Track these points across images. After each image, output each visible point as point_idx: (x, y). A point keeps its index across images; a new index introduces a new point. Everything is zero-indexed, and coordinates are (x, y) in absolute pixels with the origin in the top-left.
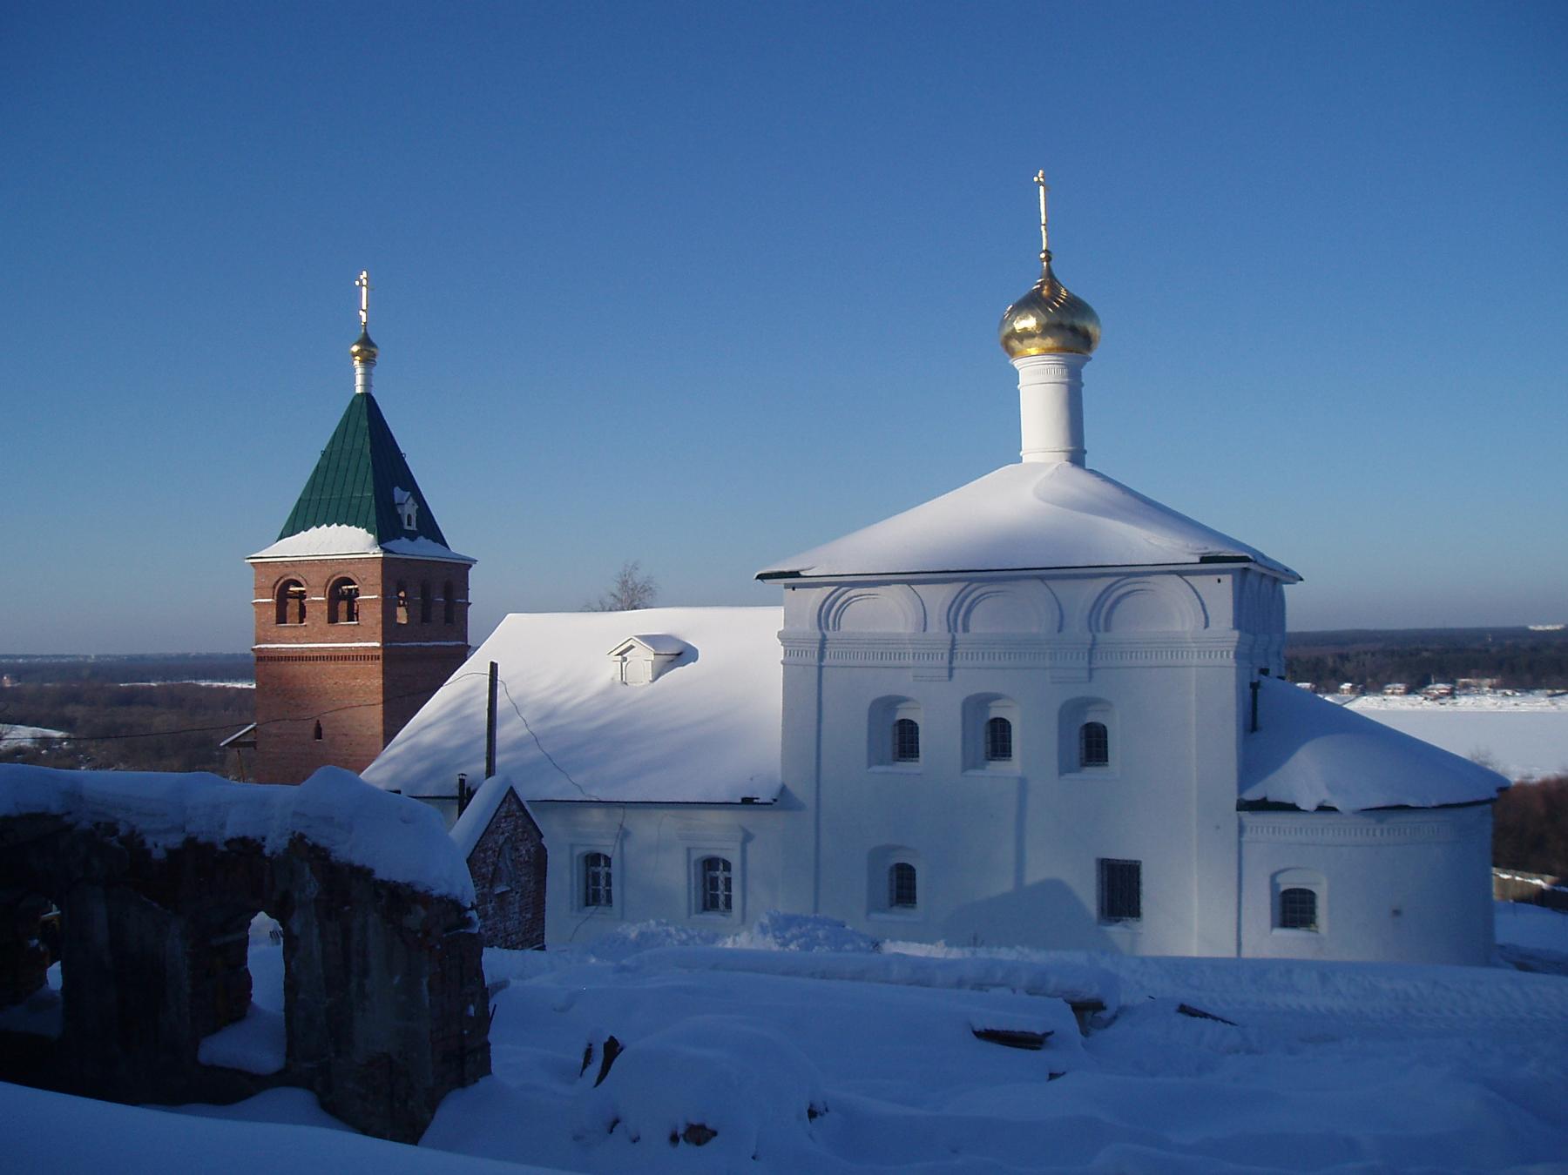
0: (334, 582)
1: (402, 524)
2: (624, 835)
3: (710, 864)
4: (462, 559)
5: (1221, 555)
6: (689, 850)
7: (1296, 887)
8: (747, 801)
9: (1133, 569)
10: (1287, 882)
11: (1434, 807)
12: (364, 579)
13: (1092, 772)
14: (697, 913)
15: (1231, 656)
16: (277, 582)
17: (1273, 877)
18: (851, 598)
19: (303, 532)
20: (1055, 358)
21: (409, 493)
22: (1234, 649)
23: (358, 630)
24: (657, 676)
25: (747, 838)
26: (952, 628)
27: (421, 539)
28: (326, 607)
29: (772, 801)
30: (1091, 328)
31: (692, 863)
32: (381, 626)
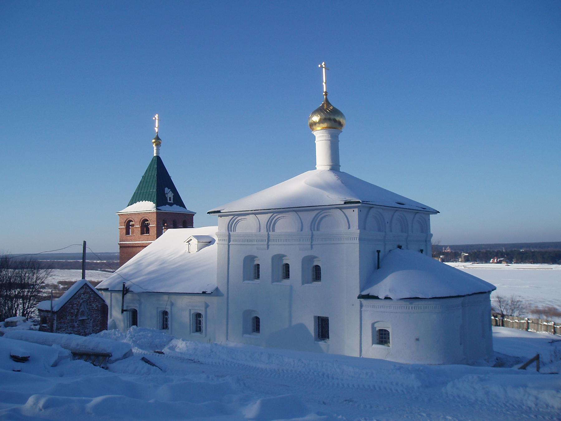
0: (144, 219)
1: (167, 200)
2: (172, 304)
3: (198, 315)
4: (190, 212)
5: (351, 201)
6: (190, 310)
7: (382, 329)
8: (204, 293)
9: (323, 207)
10: (379, 327)
11: (430, 298)
12: (151, 219)
13: (316, 283)
14: (193, 332)
15: (358, 239)
16: (126, 221)
17: (373, 325)
18: (239, 220)
19: (135, 204)
20: (325, 131)
21: (170, 190)
22: (358, 236)
23: (149, 237)
24: (199, 249)
25: (207, 306)
26: (267, 231)
27: (175, 206)
28: (140, 229)
29: (211, 293)
30: (342, 120)
31: (191, 314)
32: (156, 235)
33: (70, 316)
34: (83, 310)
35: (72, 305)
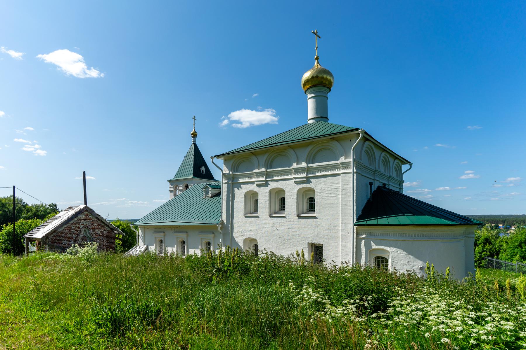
33: (67, 240)
34: (85, 235)
35: (69, 231)
